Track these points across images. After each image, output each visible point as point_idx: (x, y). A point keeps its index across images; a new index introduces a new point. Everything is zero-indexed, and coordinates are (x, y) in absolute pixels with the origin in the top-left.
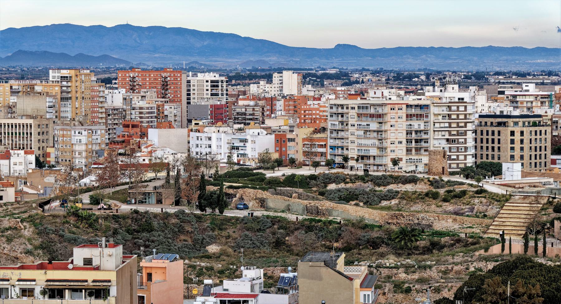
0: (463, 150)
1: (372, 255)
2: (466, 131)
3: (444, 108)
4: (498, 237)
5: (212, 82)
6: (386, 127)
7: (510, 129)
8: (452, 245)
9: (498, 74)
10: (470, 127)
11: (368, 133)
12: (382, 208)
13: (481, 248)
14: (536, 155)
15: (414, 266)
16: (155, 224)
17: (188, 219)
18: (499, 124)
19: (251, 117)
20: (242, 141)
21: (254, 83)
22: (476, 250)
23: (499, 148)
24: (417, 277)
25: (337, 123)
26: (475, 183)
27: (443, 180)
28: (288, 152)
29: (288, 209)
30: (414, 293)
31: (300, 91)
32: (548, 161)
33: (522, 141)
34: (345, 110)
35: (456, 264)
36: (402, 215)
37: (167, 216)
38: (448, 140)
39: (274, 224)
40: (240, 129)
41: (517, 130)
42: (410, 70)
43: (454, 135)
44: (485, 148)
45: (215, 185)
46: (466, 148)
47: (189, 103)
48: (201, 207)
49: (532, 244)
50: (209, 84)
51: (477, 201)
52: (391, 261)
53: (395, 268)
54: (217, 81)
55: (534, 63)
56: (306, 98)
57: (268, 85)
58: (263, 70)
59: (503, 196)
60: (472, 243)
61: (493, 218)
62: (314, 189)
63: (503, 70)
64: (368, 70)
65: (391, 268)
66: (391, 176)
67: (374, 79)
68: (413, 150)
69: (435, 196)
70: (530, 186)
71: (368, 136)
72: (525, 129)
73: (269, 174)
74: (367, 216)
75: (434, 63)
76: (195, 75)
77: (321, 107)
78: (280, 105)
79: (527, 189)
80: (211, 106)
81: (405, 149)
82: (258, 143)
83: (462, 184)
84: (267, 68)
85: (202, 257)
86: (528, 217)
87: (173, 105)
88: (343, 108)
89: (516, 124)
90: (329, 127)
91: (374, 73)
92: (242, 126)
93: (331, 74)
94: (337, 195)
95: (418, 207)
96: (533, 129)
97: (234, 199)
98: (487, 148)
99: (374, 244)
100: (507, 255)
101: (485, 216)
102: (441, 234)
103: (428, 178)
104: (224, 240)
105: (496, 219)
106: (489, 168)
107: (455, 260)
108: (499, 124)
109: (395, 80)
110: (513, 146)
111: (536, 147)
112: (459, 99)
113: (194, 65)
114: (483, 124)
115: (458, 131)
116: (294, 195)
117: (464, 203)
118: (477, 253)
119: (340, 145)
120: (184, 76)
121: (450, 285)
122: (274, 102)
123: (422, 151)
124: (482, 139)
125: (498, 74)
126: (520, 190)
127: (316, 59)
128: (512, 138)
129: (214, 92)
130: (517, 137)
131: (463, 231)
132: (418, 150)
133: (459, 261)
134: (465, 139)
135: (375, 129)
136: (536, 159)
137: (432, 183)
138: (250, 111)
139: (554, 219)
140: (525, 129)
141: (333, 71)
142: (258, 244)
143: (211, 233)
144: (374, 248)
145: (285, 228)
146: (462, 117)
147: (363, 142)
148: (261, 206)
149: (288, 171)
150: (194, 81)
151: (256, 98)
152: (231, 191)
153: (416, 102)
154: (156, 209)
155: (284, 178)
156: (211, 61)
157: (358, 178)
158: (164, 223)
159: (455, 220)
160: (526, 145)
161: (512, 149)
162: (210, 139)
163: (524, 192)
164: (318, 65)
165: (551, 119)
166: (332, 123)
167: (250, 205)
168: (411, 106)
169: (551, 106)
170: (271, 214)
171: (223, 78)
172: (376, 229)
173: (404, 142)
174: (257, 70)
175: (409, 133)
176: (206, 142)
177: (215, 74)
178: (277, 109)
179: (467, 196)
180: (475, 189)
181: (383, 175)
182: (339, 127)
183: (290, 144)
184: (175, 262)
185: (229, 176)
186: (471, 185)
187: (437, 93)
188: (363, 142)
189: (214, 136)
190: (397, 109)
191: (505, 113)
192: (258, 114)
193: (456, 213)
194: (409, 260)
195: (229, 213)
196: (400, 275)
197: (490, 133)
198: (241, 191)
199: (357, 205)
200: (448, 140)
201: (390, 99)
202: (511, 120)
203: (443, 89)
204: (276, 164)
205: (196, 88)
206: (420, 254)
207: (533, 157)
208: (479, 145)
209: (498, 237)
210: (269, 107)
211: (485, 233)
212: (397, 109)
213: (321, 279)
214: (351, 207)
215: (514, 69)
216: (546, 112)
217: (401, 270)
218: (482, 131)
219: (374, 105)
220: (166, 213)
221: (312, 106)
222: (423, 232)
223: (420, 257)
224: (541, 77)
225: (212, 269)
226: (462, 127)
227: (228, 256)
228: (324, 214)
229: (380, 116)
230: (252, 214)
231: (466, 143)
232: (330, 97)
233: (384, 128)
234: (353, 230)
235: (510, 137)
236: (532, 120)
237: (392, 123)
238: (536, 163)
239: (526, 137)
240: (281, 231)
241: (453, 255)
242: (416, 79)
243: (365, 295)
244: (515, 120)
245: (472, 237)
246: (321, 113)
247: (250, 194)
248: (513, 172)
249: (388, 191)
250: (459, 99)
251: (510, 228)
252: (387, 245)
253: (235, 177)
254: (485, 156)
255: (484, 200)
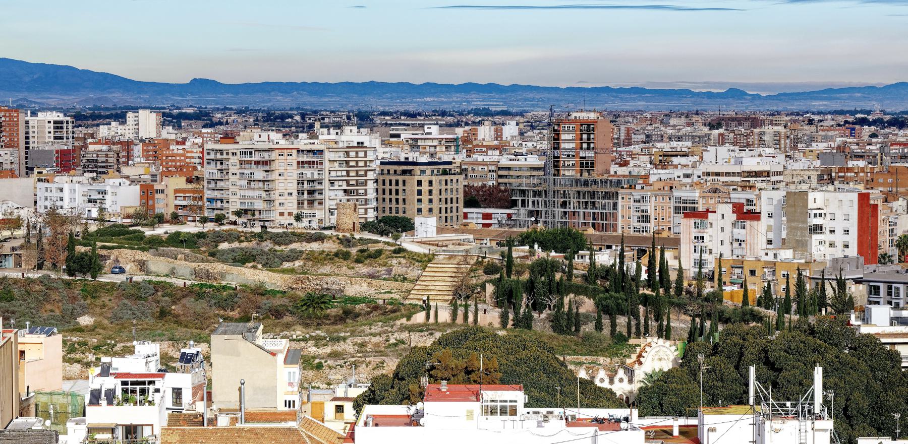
0: (363, 203)
1: (275, 325)
2: (366, 181)
3: (341, 154)
4: (421, 303)
5: (55, 122)
6: (274, 176)
7: (417, 178)
8: (369, 313)
9: (384, 114)
10: (371, 175)
11: (252, 183)
12: (284, 271)
13: (403, 316)
14: (446, 208)
15: (325, 338)
16: (15, 291)
17: (55, 285)
18: (404, 172)
19: (104, 164)
20: (99, 192)
21: (104, 124)
22: (397, 318)
23: (404, 200)
24: (329, 351)
25: (216, 171)
26: (390, 240)
27: (354, 238)
28: (156, 206)
29: (173, 273)
30: (326, 370)
31: (159, 133)
32: (461, 214)
33: (430, 192)
34: (225, 156)
35: (374, 335)
36: (308, 279)
37: (30, 281)
38: (345, 191)
39: (157, 291)
40: (93, 179)
41: (425, 179)
42: (290, 109)
43: (353, 185)
44: (387, 200)
45: (85, 245)
46: (366, 200)
47: (27, 148)
48: (71, 272)
49: (460, 312)
50: (52, 125)
51: (394, 261)
52: (299, 333)
53: (303, 340)
54: (62, 122)
55: (422, 102)
56: (167, 143)
57: (121, 127)
58: (107, 109)
59: (425, 255)
60: (391, 311)
61: (414, 281)
62: (203, 249)
63: (387, 109)
64: (231, 109)
65: (299, 340)
66: (294, 234)
67: (240, 119)
68: (306, 202)
69: (346, 256)
70: (453, 244)
71: (252, 186)
72: (433, 178)
73: (148, 232)
74: (266, 280)
75: (309, 101)
76: (34, 114)
77: (188, 152)
78: (137, 150)
79: (451, 247)
80: (57, 151)
81: (295, 202)
82: (121, 197)
83: (377, 242)
84: (111, 106)
85: (73, 330)
86: (456, 279)
87: (9, 151)
88: (222, 154)
89: (423, 172)
90: (206, 176)
91: (239, 112)
92: (95, 174)
93: (190, 114)
94: (230, 256)
95: (327, 269)
96: (444, 178)
97: (108, 262)
98: (390, 200)
99: (277, 313)
100: (433, 324)
101: (405, 279)
102: (354, 300)
103: (337, 236)
104: (98, 310)
105: (418, 282)
106: (393, 224)
107: (373, 331)
108: (404, 172)
109: (264, 121)
110: (420, 197)
111: (446, 199)
112: (358, 143)
113: (23, 103)
114: (385, 172)
115: (357, 181)
116: (180, 256)
117: (379, 264)
118: (398, 323)
119: (219, 197)
120: (22, 116)
121: (368, 359)
122: (132, 147)
123: (316, 203)
124: (384, 190)
125: (384, 114)
126: (444, 248)
127: (168, 95)
128: (419, 188)
129: (58, 134)
130: (425, 187)
131: (380, 296)
132: (310, 202)
133: (377, 331)
134: (366, 190)
135: (261, 178)
136: (446, 212)
137: (341, 241)
138: (102, 157)
139: (485, 282)
140: (433, 178)
141: (190, 111)
142: (139, 314)
143: (82, 302)
144: (277, 318)
145: (171, 296)
146: (361, 164)
147: (247, 193)
148: (141, 270)
149: (172, 229)
150: (33, 121)
151: (108, 142)
152: (104, 252)
153: (309, 147)
154: (16, 275)
155: (166, 236)
156: (42, 98)
157: (254, 235)
158: (27, 291)
159: (370, 284)
160: (435, 197)
161: (419, 201)
162: (61, 190)
163: (449, 251)
164: (170, 103)
165: (460, 167)
166: (208, 171)
167: (127, 268)
168: (303, 151)
169: (457, 152)
170: (153, 278)
171: (69, 119)
172: (279, 295)
173: (295, 193)
174: (99, 108)
175: (301, 182)
176: (56, 194)
177: (59, 114)
178: (135, 155)
179: (383, 256)
180: (393, 248)
181: (284, 232)
182: (218, 176)
183: (157, 196)
184: (52, 337)
185: (101, 234)
186: (388, 244)
187: (333, 136)
188: (247, 193)
189: (66, 187)
190: (286, 154)
191: (410, 160)
192: (112, 159)
193: (372, 276)
194: (318, 332)
195: (102, 279)
196: (309, 349)
197: (394, 183)
198: (116, 252)
199: (254, 267)
200: (345, 191)
201: (277, 143)
202: (418, 167)
203: (339, 131)
204: (156, 220)
205: (35, 130)
206: (333, 324)
207: (443, 211)
208: (381, 196)
209: (421, 303)
210: (124, 153)
211: (405, 298)
212: (286, 154)
213: (238, 355)
214: (248, 270)
215: (402, 109)
216: (454, 159)
217: (310, 343)
218: (384, 181)
219: (259, 150)
220: (29, 278)
221: (175, 152)
222: (334, 298)
223: (331, 328)
224: (434, 118)
225: (85, 344)
226: (362, 176)
227: (104, 329)
228: (215, 278)
229: (266, 163)
230: (131, 279)
231: (366, 195)
232: (196, 142)
233: (271, 176)
234: (251, 296)
235: (417, 188)
236: (442, 167)
237: (281, 172)
238: (446, 218)
239: (435, 188)
240: (167, 298)
241: (371, 325)
242: (290, 120)
243: (290, 373)
244: (422, 167)
245: (391, 304)
246: (188, 160)
247: (127, 257)
248: (427, 227)
249: (291, 250)
250: (358, 143)
251: (435, 293)
252: (292, 313)
253: (109, 235)
254: (387, 210)
255: (403, 261)
